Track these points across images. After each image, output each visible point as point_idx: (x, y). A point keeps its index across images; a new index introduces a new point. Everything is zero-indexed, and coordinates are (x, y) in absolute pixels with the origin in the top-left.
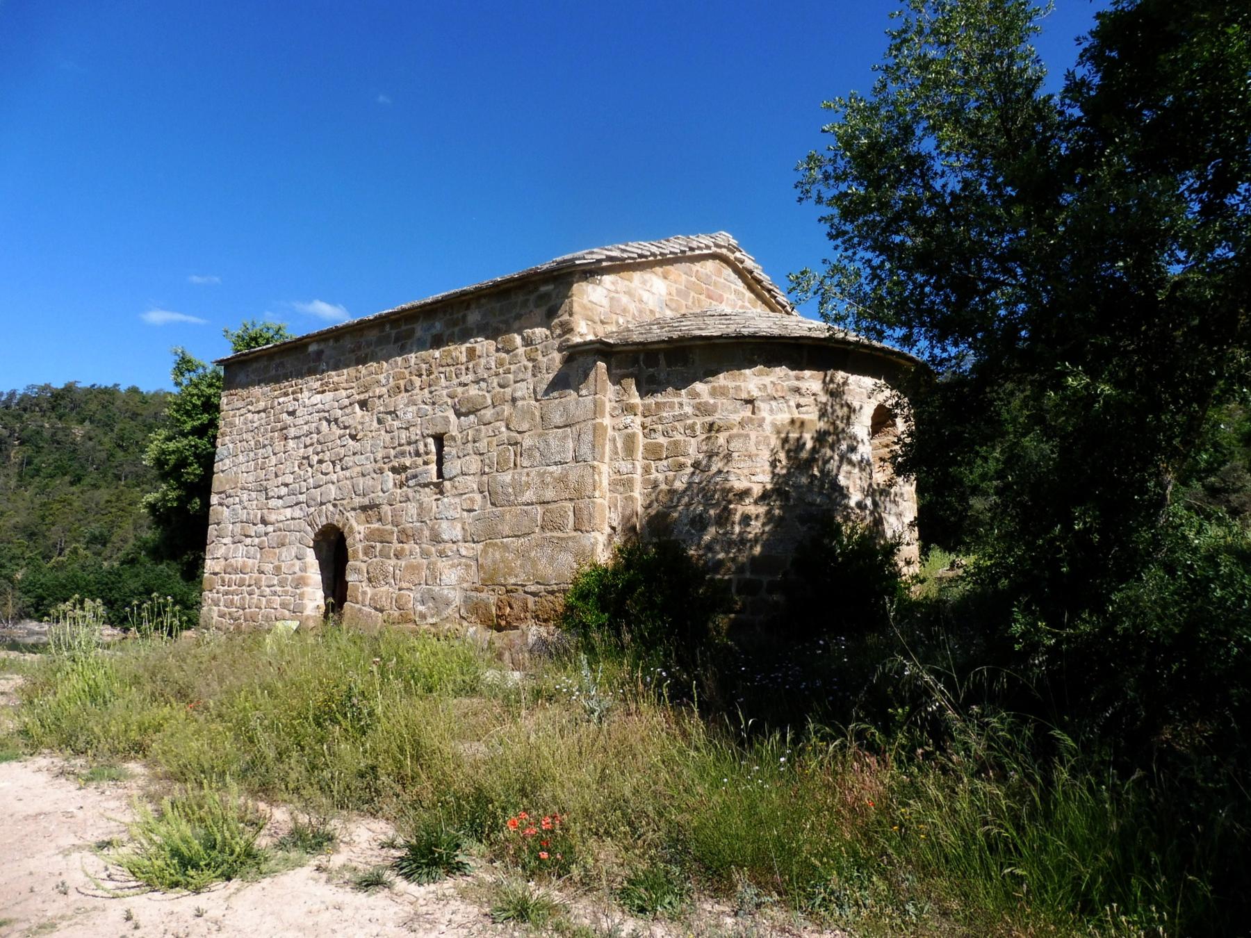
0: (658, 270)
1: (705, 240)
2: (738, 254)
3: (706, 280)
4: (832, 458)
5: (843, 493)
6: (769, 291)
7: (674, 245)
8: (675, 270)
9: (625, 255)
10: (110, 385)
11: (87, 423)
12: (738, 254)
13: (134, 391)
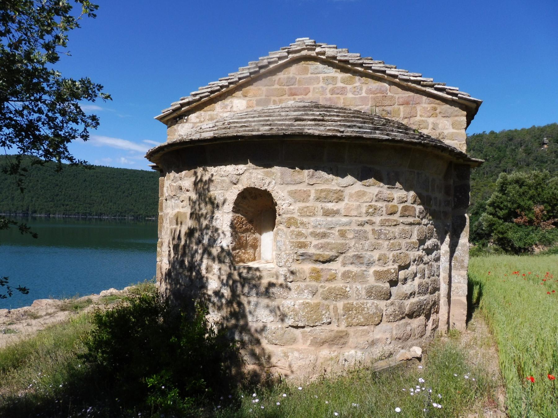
0: (239, 93)
1: (274, 55)
2: (318, 50)
3: (290, 81)
4: (196, 251)
5: (201, 283)
6: (361, 65)
7: (244, 72)
8: (252, 89)
9: (198, 97)
10: (481, 132)
11: (472, 151)
12: (318, 50)
13: (492, 133)
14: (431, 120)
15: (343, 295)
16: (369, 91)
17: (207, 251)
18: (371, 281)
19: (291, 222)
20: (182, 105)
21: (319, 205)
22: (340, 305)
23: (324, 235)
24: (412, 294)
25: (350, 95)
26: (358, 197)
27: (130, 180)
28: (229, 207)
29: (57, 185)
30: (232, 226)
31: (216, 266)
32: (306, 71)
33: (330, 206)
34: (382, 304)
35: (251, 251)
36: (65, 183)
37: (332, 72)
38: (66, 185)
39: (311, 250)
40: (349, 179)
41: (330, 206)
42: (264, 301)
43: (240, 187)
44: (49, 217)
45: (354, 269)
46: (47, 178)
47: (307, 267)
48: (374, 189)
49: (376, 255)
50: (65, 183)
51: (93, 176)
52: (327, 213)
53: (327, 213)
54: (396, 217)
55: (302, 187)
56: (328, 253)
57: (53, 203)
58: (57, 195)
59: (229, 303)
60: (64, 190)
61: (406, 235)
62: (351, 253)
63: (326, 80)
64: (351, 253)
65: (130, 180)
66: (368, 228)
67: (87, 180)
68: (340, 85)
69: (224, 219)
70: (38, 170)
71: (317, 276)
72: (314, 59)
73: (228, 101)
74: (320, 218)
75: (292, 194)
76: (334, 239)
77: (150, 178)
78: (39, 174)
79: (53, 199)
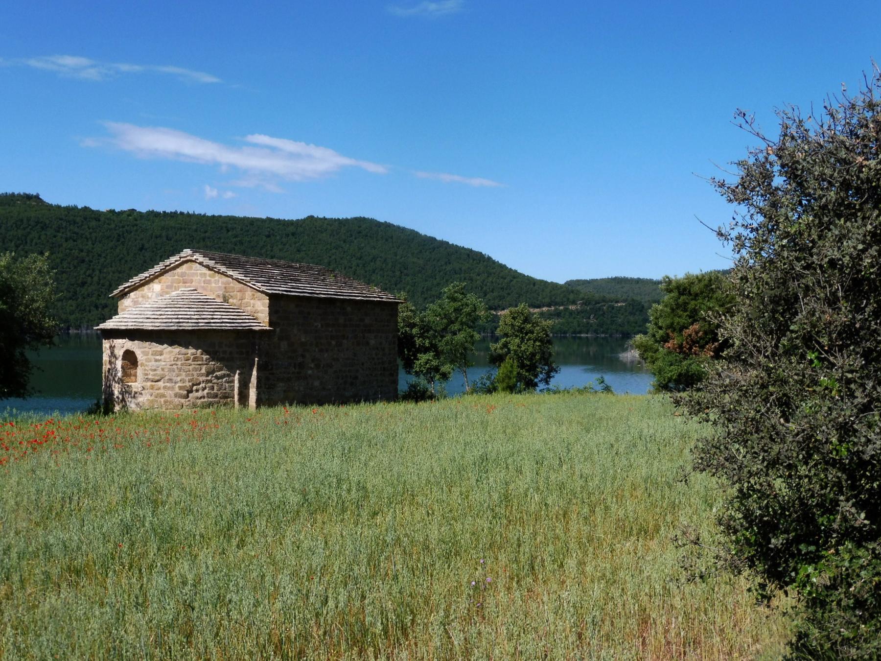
0: (156, 281)
1: (173, 259)
3: (183, 275)
14: (252, 301)
15: (163, 396)
16: (223, 283)
17: (114, 379)
18: (177, 390)
19: (142, 365)
20: (125, 288)
21: (153, 357)
22: (162, 400)
23: (155, 370)
24: (204, 397)
25: (213, 285)
26: (169, 353)
27: (241, 243)
28: (121, 358)
29: (83, 261)
30: (122, 367)
31: (117, 385)
32: (191, 268)
33: (157, 357)
34: (183, 401)
35: (133, 378)
36: (100, 255)
37: (205, 271)
38: (103, 260)
39: (150, 377)
40: (165, 346)
41: (157, 357)
42: (133, 400)
43: (124, 349)
44: (69, 334)
45: (168, 384)
46: (60, 246)
47: (149, 384)
48: (177, 350)
49: (179, 379)
50: (100, 255)
51: (160, 236)
52: (156, 361)
53: (156, 361)
54: (190, 362)
55: (146, 350)
56: (157, 378)
57: (74, 303)
58: (83, 284)
59: (122, 401)
60: (97, 272)
61: (195, 370)
62: (167, 378)
63: (201, 274)
64: (167, 378)
65: (241, 243)
66: (175, 367)
67: (147, 246)
68: (208, 278)
69: (119, 364)
70: (42, 228)
71: (152, 387)
72: (194, 261)
73: (151, 285)
74: (153, 363)
75: (143, 352)
76: (159, 372)
77: (287, 235)
78: (43, 237)
79: (75, 293)
